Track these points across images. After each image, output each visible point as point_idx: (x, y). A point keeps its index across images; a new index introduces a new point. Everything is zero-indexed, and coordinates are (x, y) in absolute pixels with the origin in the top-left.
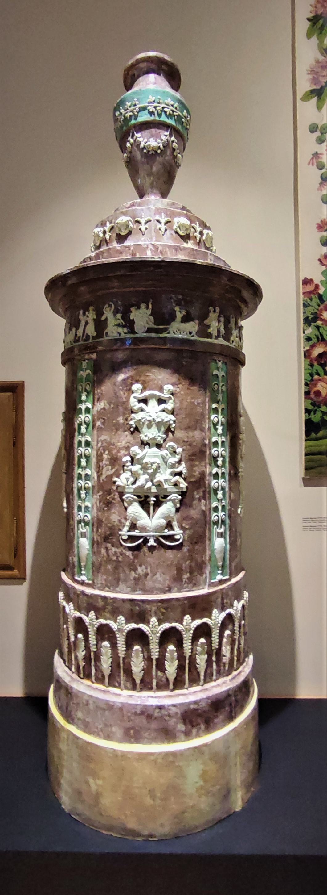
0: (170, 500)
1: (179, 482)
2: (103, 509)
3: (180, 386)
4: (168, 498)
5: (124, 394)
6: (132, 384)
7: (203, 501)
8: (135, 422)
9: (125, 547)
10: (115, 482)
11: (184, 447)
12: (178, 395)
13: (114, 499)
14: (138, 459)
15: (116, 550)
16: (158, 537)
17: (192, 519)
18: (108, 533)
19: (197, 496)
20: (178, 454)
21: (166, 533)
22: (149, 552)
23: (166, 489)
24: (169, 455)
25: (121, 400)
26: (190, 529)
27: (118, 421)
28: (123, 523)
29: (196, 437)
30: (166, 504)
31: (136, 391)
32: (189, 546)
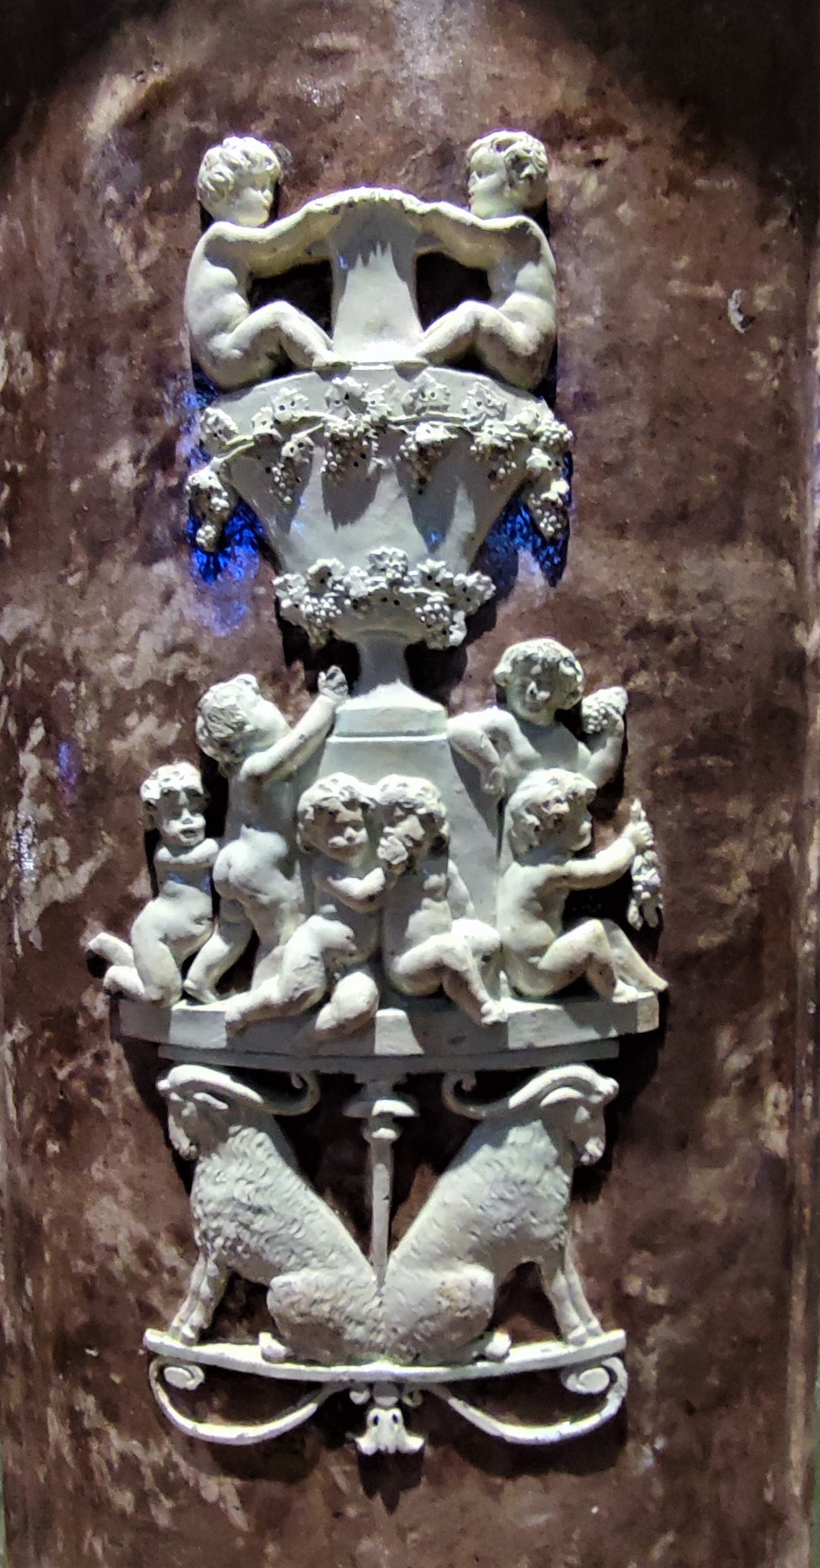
0: (530, 1111)
1: (607, 972)
2: (41, 1148)
3: (612, 151)
4: (517, 1099)
5: (140, 242)
6: (198, 144)
7: (776, 1094)
8: (226, 472)
9: (192, 1443)
10: (99, 963)
11: (641, 680)
12: (594, 228)
13: (97, 1085)
14: (257, 779)
15: (134, 1446)
16: (441, 1393)
17: (696, 1231)
18: (79, 1317)
19: (738, 1061)
20: (592, 740)
21: (500, 1359)
22: (370, 1493)
23: (499, 1028)
24: (524, 746)
25: (116, 302)
26: (675, 1309)
27: (104, 481)
28: (173, 1271)
29: (731, 597)
30: (498, 1142)
31: (237, 189)
32: (669, 1430)
